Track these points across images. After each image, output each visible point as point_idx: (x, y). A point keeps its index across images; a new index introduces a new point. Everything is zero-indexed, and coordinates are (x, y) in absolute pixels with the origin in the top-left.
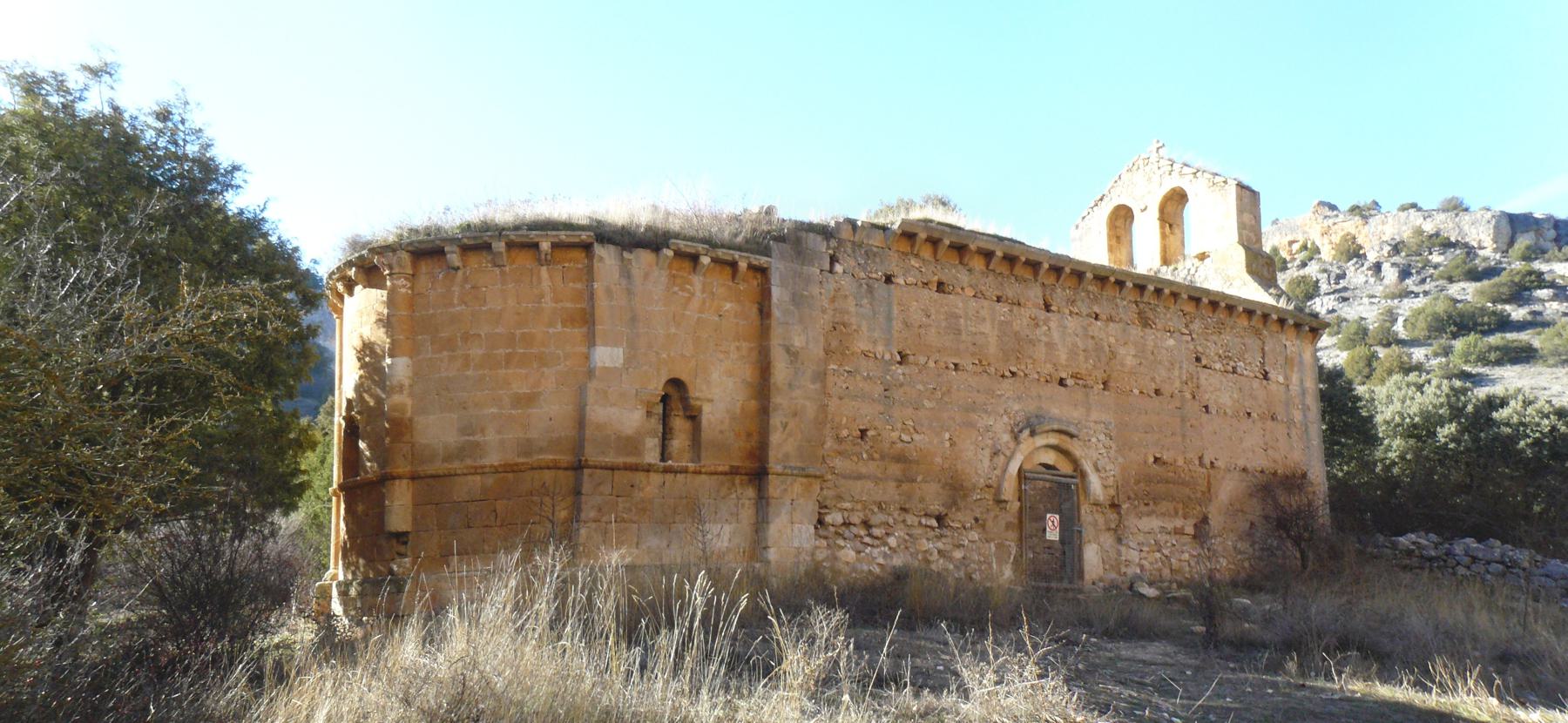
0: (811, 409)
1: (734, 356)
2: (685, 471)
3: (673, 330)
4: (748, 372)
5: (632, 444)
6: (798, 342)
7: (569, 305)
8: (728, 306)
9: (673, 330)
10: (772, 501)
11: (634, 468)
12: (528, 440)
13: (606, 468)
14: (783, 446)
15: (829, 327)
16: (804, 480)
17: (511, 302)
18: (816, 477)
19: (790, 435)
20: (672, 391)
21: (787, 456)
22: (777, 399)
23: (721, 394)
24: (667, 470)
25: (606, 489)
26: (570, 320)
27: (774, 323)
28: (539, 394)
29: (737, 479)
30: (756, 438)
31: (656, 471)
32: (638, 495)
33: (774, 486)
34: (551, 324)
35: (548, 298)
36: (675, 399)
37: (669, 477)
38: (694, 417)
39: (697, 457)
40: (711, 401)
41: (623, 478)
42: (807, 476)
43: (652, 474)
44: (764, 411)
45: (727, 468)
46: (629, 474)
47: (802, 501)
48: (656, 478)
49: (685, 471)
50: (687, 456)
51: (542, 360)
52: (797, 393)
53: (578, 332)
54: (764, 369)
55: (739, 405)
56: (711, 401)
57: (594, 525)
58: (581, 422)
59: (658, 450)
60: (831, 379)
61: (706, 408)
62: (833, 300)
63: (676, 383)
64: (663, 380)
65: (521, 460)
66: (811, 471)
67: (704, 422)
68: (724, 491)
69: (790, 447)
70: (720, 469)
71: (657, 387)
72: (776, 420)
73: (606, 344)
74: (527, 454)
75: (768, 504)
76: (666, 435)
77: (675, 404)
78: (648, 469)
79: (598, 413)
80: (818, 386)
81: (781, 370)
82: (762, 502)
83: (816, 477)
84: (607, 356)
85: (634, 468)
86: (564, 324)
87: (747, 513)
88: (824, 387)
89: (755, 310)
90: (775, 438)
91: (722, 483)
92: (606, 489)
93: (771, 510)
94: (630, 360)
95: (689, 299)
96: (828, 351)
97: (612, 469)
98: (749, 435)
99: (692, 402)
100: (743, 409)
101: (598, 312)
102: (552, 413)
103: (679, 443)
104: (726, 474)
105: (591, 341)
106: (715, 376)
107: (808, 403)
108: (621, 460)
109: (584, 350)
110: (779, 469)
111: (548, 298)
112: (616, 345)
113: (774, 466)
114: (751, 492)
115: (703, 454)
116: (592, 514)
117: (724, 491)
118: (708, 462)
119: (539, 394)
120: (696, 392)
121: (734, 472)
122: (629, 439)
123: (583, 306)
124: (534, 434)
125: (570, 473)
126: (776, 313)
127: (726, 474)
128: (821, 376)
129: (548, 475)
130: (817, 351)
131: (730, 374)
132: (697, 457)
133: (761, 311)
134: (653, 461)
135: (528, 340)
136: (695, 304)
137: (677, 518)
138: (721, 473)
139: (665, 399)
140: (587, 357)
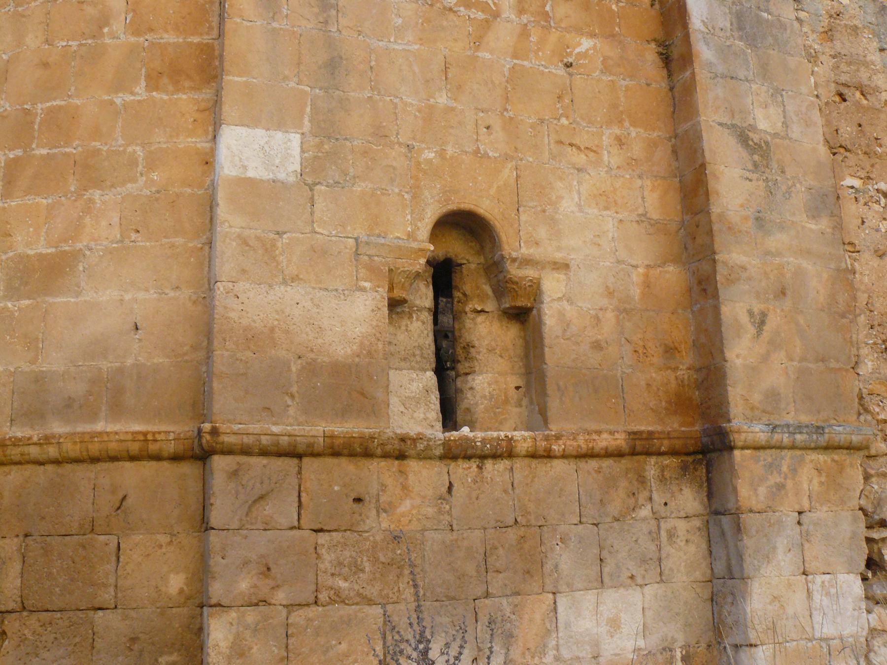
0: (817, 282)
1: (612, 157)
2: (504, 452)
3: (442, 99)
4: (651, 197)
5: (352, 383)
6: (765, 121)
7: (170, 38)
8: (586, 44)
9: (442, 99)
10: (748, 519)
11: (361, 450)
12: (39, 379)
13: (281, 453)
14: (759, 375)
15: (828, 93)
16: (822, 458)
17: (33, 41)
18: (850, 448)
19: (774, 344)
20: (456, 248)
21: (773, 395)
22: (733, 255)
23: (587, 247)
24: (452, 454)
25: (281, 509)
26: (168, 72)
27: (702, 76)
28: (75, 256)
29: (652, 467)
30: (687, 359)
31: (424, 456)
32: (377, 525)
33: (751, 480)
34: (120, 84)
35: (118, 25)
36: (462, 270)
37: (464, 471)
38: (522, 314)
39: (539, 415)
40: (563, 266)
41: (325, 478)
42: (828, 448)
43: (413, 465)
44: (704, 291)
45: (620, 441)
46: (346, 466)
47: (822, 513)
48: (425, 477)
49: (504, 452)
50: (514, 413)
51: (91, 173)
52: (777, 240)
53: (187, 100)
54: (692, 187)
55: (636, 277)
56: (563, 266)
57: (252, 616)
58: (206, 328)
59: (435, 398)
60: (852, 210)
61: (552, 286)
62: (828, 34)
63: (464, 224)
64: (431, 214)
65: (19, 432)
66: (840, 433)
67: (552, 315)
68: (617, 502)
69: (778, 375)
70: (604, 441)
71: (410, 232)
72: (736, 308)
73: (252, 122)
74: (33, 413)
75: (738, 528)
76: (448, 362)
77: (472, 283)
78: (401, 451)
79: (251, 301)
80: (824, 224)
81: (733, 188)
82: (721, 517)
83: (850, 448)
84: (254, 151)
85: (361, 450)
86: (153, 81)
87: (685, 555)
88: (839, 226)
89: (651, 54)
90: (739, 353)
91: (610, 482)
92: (281, 509)
93: (749, 543)
94: (314, 168)
95: (486, 25)
96: (836, 148)
97: (295, 453)
98: (670, 351)
99: (515, 271)
100: (647, 284)
101: (234, 44)
102: (115, 306)
103: (489, 380)
104: (617, 454)
105: (213, 119)
106: (568, 205)
107: (806, 264)
108: (317, 429)
109: (203, 145)
110: (758, 432)
111: (118, 25)
112: (281, 125)
113: (745, 426)
114: (689, 499)
115: (554, 405)
116: (244, 585)
117: (617, 502)
118: (569, 426)
119: (75, 256)
120: (524, 241)
121: (640, 448)
122: (341, 371)
123: (206, 39)
124: (53, 362)
125: (188, 469)
126: (704, 53)
127: (617, 454)
128: (828, 202)
129: (131, 475)
130: (810, 141)
131: (606, 200)
132: (539, 415)
133: (666, 59)
134: (411, 428)
135: (60, 124)
136: (503, 35)
137: (497, 583)
138: (608, 454)
139: (443, 276)
140: (208, 161)
